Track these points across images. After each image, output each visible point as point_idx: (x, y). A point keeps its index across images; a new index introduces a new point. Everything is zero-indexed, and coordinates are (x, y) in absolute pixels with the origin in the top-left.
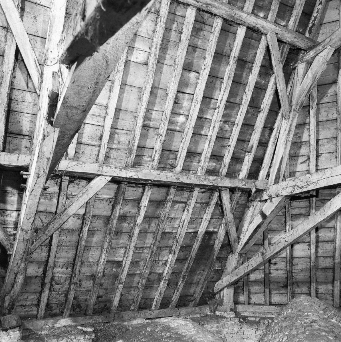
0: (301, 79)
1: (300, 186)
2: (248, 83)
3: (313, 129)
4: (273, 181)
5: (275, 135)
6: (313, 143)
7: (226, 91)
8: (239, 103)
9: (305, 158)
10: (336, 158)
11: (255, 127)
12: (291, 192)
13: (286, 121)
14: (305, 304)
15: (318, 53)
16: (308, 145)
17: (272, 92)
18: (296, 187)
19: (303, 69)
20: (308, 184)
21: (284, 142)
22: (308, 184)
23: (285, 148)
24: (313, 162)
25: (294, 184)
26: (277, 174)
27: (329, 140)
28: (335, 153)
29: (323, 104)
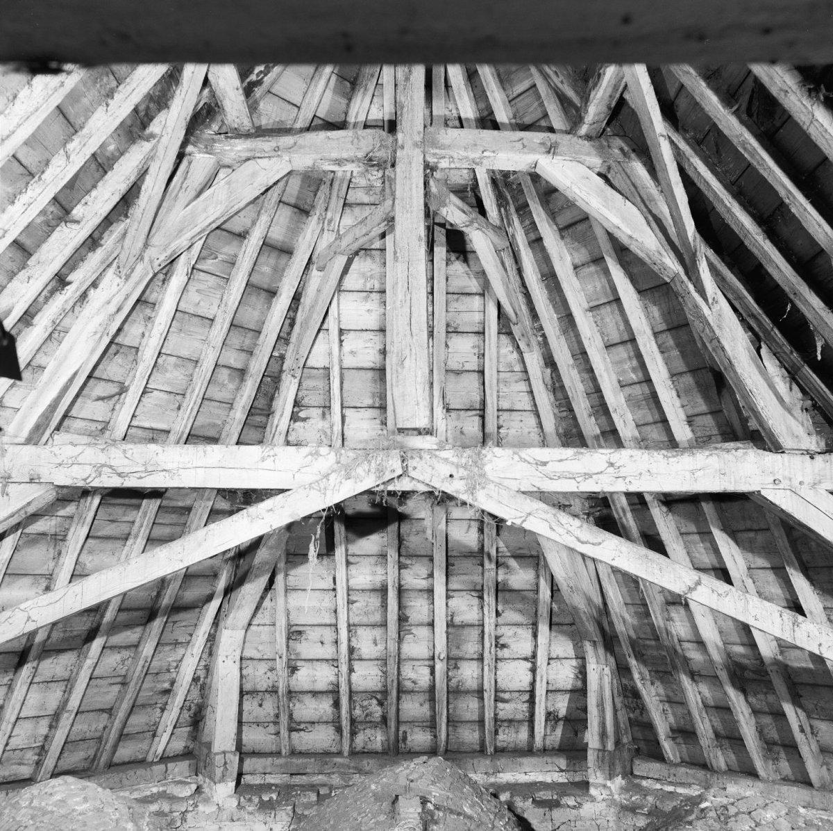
0: (193, 194)
1: (120, 470)
2: (85, 131)
3: (163, 323)
4: (25, 433)
5: (66, 301)
6: (148, 355)
7: (33, 118)
8: (34, 170)
9: (112, 389)
10: (179, 408)
11: (33, 259)
12: (85, 480)
13: (118, 280)
14: (79, 808)
15: (257, 155)
16: (131, 358)
17: (123, 187)
18: (105, 469)
19: (206, 170)
20: (146, 471)
21: (95, 333)
22: (146, 471)
23: (71, 349)
24: (131, 406)
25: (102, 458)
26: (43, 415)
27: (179, 362)
28: (179, 398)
29: (202, 274)
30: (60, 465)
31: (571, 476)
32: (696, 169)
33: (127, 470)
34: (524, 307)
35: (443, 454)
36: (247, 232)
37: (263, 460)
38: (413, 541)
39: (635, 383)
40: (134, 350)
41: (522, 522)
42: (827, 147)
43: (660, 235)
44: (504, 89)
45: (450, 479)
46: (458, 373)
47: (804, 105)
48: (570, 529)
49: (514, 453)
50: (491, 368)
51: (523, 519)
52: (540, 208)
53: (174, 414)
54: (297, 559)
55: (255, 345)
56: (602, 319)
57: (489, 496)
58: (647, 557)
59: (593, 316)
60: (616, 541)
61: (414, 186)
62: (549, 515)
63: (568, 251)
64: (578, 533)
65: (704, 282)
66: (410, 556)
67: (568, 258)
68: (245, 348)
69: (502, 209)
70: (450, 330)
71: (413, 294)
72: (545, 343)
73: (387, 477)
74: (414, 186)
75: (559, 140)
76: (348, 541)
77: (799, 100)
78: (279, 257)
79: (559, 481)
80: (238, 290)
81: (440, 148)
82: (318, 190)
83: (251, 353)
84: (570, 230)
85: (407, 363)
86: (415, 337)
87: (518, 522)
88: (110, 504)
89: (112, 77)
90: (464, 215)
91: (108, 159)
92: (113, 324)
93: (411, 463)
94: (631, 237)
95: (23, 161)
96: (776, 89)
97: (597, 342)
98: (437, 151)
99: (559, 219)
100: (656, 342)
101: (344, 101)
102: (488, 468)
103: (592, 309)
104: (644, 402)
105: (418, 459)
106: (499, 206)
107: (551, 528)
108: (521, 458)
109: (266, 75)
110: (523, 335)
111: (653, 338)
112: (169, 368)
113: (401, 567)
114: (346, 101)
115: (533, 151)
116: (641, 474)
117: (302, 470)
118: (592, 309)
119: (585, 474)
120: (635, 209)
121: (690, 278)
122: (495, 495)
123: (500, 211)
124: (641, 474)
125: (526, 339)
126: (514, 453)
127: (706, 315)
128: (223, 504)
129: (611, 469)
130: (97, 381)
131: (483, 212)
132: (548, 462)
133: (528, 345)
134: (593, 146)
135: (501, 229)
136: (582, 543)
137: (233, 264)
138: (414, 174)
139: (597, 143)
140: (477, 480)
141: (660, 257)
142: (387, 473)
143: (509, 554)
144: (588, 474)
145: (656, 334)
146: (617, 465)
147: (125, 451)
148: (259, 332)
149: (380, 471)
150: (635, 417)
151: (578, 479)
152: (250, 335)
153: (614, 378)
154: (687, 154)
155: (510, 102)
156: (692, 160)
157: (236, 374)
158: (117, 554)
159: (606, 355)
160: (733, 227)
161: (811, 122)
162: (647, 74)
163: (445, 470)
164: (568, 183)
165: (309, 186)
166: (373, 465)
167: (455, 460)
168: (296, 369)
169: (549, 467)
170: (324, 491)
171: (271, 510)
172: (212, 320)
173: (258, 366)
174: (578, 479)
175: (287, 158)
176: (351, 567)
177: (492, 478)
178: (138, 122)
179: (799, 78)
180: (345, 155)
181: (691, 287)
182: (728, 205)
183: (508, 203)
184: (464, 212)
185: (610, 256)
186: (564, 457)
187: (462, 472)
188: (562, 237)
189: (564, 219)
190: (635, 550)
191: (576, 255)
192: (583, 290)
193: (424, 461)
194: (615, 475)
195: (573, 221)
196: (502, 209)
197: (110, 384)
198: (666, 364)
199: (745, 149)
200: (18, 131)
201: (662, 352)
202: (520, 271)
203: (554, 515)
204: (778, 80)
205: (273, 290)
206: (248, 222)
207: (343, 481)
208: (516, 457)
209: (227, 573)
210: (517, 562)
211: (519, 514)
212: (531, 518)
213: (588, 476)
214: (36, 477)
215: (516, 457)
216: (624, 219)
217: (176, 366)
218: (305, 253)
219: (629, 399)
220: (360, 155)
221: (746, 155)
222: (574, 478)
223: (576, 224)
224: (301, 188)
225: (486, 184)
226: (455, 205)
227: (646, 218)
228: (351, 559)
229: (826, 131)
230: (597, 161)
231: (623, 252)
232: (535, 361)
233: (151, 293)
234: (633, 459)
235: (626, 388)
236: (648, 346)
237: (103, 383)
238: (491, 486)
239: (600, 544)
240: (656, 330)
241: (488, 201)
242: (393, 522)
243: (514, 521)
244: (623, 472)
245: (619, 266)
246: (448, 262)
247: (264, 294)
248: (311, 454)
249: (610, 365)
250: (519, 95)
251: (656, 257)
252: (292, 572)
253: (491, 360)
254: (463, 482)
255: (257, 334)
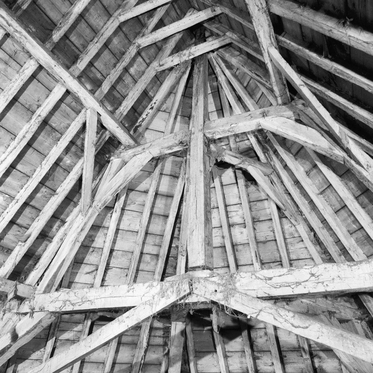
0: (113, 175)
1: (73, 302)
3: (111, 235)
7: (14, 152)
8: (29, 174)
9: (93, 268)
10: (127, 276)
16: (100, 253)
21: (72, 241)
25: (67, 297)
26: (51, 279)
27: (124, 253)
28: (126, 270)
29: (129, 211)
30: (52, 302)
31: (287, 285)
32: (330, 97)
33: (75, 302)
34: (289, 201)
35: (213, 279)
36: (148, 190)
37: (128, 291)
38: (260, 341)
39: (357, 230)
40: (101, 249)
41: (257, 316)
42: (363, 48)
43: (330, 139)
44: (253, 98)
45: (215, 293)
46: (264, 242)
47: (341, 32)
48: (287, 318)
49: (252, 274)
50: (279, 237)
51: (257, 313)
52: (280, 148)
53: (125, 279)
54: (201, 355)
55: (162, 242)
56: (328, 197)
57: (236, 301)
58: (342, 336)
59: (324, 197)
60: (319, 325)
61: (199, 149)
62: (273, 310)
63: (301, 165)
64: (292, 321)
65: (356, 157)
66: (259, 352)
67: (302, 169)
68: (157, 244)
69: (266, 154)
70: (255, 221)
71: (198, 198)
72: (306, 220)
73: (182, 294)
74: (199, 149)
75: (269, 110)
76: (224, 343)
77: (338, 31)
78: (166, 200)
79: (281, 288)
80: (146, 216)
81: (211, 129)
82: (181, 166)
83: (160, 246)
84: (299, 155)
85: (194, 233)
86: (198, 219)
87: (254, 316)
88: (98, 325)
89: (57, 133)
90: (237, 159)
91: (69, 167)
92: (81, 237)
93: (195, 286)
94: (313, 145)
95: (22, 171)
96: (327, 32)
97: (328, 211)
98: (209, 131)
99: (293, 151)
100: (359, 203)
101: (186, 126)
102: (238, 285)
103: (321, 193)
104: (365, 241)
105: (198, 283)
106: (264, 153)
107: (275, 319)
108: (256, 277)
109: (143, 122)
110: (291, 216)
111: (355, 201)
112: (120, 257)
113: (255, 359)
114: (188, 125)
115: (256, 118)
116: (333, 279)
117: (145, 295)
118: (321, 193)
119: (297, 283)
120: (314, 131)
121: (351, 158)
122: (240, 300)
123: (265, 155)
124: (333, 279)
125: (293, 218)
126: (252, 274)
127: (365, 176)
128: (159, 324)
129: (313, 278)
130: (86, 265)
131: (259, 159)
132: (272, 278)
133: (296, 221)
134: (287, 107)
135: (269, 164)
136: (296, 327)
137: (144, 205)
138: (199, 143)
139: (290, 105)
140: (231, 291)
141: (331, 151)
142: (182, 292)
143: (318, 349)
144: (298, 283)
145: (357, 198)
146: (317, 275)
147: (75, 293)
148: (163, 236)
149: (179, 291)
150: (364, 251)
151: (293, 286)
152: (158, 237)
153: (345, 230)
154: (323, 91)
155: (257, 103)
156: (326, 93)
157: (154, 257)
158: (105, 351)
159: (337, 217)
160: (361, 120)
161: (350, 39)
162: (283, 59)
163: (212, 287)
164: (276, 128)
165: (176, 165)
166: (175, 288)
167: (219, 282)
168: (183, 251)
169: (274, 280)
170: (151, 305)
171: (128, 317)
172: (138, 232)
173: (164, 251)
174: (293, 286)
175: (148, 152)
176: (229, 359)
177: (240, 291)
178: (80, 150)
179: (336, 20)
180: (170, 144)
181: (353, 162)
182: (352, 109)
183: (268, 150)
184: (236, 157)
185: (318, 161)
186: (282, 273)
187: (221, 288)
188: (296, 159)
189: (294, 150)
190: (333, 331)
191: (305, 166)
192: (314, 184)
193: (201, 284)
194: (316, 281)
195: (298, 149)
196: (266, 154)
197: (92, 266)
198: (369, 214)
199: (338, 73)
200: (8, 157)
201: (364, 208)
202: (282, 182)
203: (276, 310)
204: (325, 27)
205: (167, 215)
206: (148, 186)
207: (161, 299)
208: (254, 277)
209: (165, 362)
210: (325, 354)
211: (257, 311)
212: (262, 313)
213: (298, 284)
214: (42, 308)
215: (254, 277)
216: (308, 137)
217: (122, 255)
218: (178, 195)
219: (357, 241)
220: (177, 142)
221: (341, 76)
222: (290, 286)
223: (299, 151)
224: (172, 166)
225: (256, 144)
226: (229, 155)
227: (320, 133)
228: (228, 354)
229: (357, 39)
230: (290, 113)
231: (324, 159)
232: (303, 229)
233: (106, 223)
234: (327, 270)
235: (354, 234)
236: (352, 205)
237: (88, 266)
238: (237, 295)
239: (307, 327)
240: (356, 196)
241: (259, 152)
242: (244, 330)
243: (252, 315)
244: (321, 279)
245: (323, 165)
246: (247, 186)
247: (162, 218)
248: (149, 286)
249: (340, 223)
250: (259, 99)
251: (330, 152)
252: (200, 362)
253: (278, 232)
254: (221, 294)
255: (162, 237)
